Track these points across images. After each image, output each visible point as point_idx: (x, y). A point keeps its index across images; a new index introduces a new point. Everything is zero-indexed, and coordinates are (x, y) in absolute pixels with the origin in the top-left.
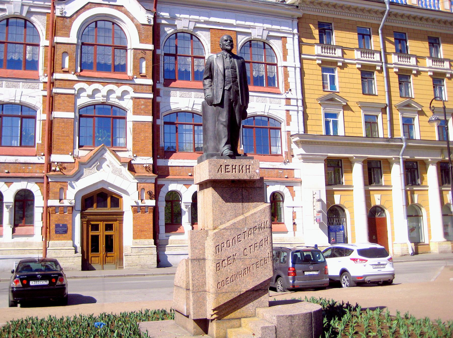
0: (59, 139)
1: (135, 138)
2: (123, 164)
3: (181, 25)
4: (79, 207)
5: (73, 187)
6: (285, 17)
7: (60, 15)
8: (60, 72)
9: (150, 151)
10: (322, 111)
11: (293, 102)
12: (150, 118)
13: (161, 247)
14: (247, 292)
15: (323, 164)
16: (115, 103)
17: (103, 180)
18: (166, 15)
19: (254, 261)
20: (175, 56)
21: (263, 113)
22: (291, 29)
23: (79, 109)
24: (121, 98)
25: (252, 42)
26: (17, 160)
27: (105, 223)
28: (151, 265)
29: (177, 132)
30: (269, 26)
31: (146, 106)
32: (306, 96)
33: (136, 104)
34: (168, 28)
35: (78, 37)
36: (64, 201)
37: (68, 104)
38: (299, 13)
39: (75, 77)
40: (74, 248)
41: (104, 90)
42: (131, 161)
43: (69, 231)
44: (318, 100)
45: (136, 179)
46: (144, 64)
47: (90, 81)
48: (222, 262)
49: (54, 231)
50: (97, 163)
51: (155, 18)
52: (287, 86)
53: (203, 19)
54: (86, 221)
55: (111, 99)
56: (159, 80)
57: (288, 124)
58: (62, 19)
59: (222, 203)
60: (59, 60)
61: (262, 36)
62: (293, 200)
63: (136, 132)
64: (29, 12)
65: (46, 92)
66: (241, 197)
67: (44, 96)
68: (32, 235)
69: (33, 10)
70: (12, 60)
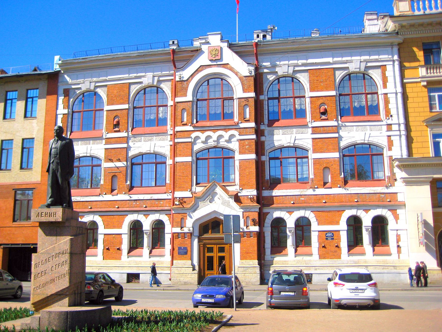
0: (180, 179)
1: (241, 174)
2: (230, 196)
3: (280, 71)
4: (197, 233)
5: (191, 217)
6: (383, 46)
7: (179, 80)
8: (180, 126)
9: (254, 184)
10: (429, 133)
11: (395, 127)
12: (253, 156)
13: (266, 267)
14: (52, 295)
15: (429, 186)
16: (224, 146)
17: (215, 211)
18: (267, 64)
19: (56, 275)
20: (278, 98)
21: (363, 141)
22: (390, 56)
23: (196, 154)
24: (229, 141)
25: (351, 75)
26: (152, 197)
27: (218, 246)
28: (254, 282)
29: (281, 165)
30: (367, 57)
31: (250, 146)
32: (410, 119)
33: (241, 145)
34: (270, 76)
35: (193, 96)
36: (184, 228)
37: (187, 150)
38: (398, 40)
39: (191, 128)
40: (192, 266)
41: (215, 136)
42: (237, 193)
43: (189, 253)
44: (424, 122)
45: (241, 208)
46: (248, 110)
47: (203, 129)
48: (38, 274)
49: (177, 252)
50: (210, 197)
51: (257, 69)
52: (388, 112)
53: (300, 62)
54: (203, 245)
55: (221, 143)
56: (263, 122)
57: (390, 149)
58: (181, 82)
59: (44, 237)
60: (179, 116)
61: (360, 68)
62: (397, 223)
63: (242, 169)
64: (159, 81)
65: (172, 142)
66: (55, 233)
67: (171, 145)
68: (163, 256)
69: (161, 79)
70: (150, 120)
